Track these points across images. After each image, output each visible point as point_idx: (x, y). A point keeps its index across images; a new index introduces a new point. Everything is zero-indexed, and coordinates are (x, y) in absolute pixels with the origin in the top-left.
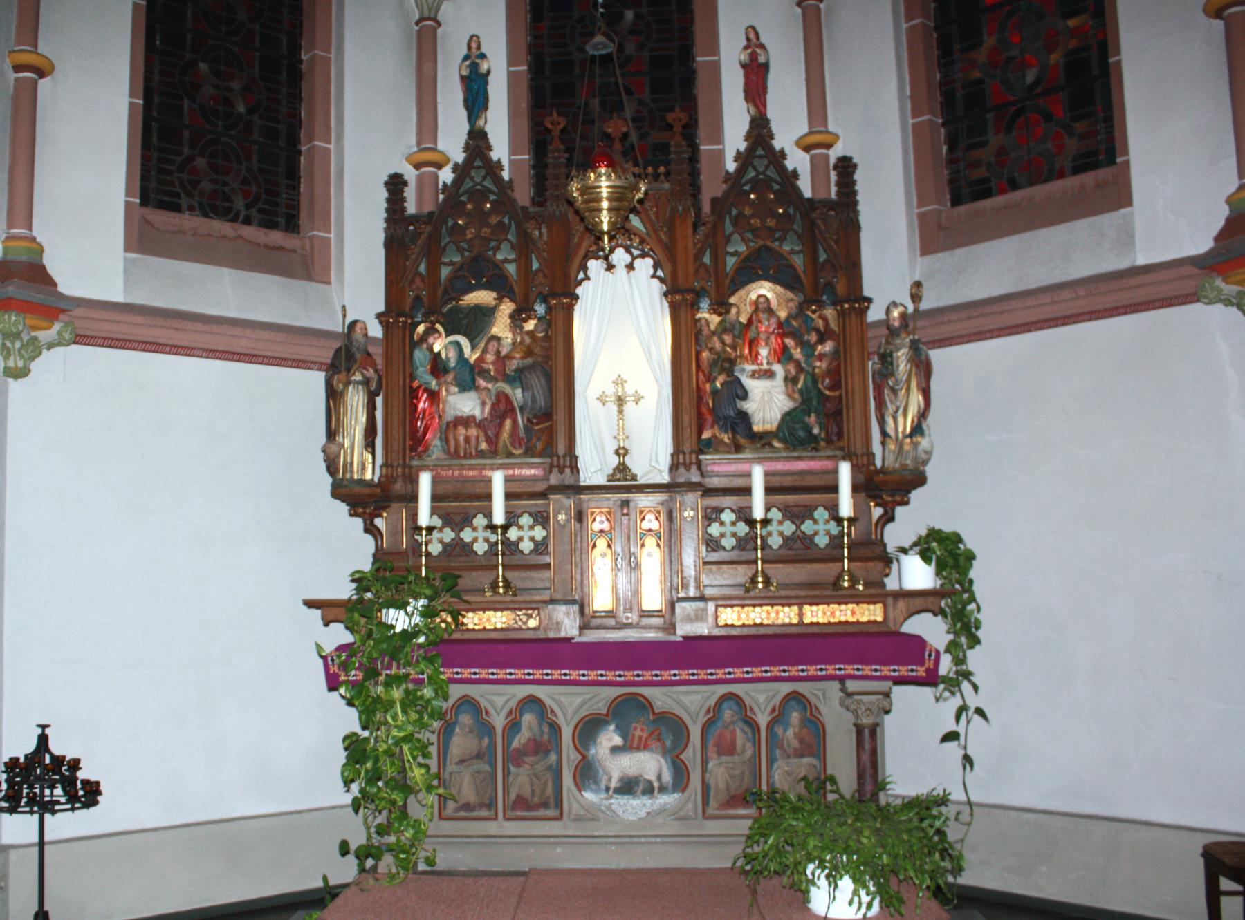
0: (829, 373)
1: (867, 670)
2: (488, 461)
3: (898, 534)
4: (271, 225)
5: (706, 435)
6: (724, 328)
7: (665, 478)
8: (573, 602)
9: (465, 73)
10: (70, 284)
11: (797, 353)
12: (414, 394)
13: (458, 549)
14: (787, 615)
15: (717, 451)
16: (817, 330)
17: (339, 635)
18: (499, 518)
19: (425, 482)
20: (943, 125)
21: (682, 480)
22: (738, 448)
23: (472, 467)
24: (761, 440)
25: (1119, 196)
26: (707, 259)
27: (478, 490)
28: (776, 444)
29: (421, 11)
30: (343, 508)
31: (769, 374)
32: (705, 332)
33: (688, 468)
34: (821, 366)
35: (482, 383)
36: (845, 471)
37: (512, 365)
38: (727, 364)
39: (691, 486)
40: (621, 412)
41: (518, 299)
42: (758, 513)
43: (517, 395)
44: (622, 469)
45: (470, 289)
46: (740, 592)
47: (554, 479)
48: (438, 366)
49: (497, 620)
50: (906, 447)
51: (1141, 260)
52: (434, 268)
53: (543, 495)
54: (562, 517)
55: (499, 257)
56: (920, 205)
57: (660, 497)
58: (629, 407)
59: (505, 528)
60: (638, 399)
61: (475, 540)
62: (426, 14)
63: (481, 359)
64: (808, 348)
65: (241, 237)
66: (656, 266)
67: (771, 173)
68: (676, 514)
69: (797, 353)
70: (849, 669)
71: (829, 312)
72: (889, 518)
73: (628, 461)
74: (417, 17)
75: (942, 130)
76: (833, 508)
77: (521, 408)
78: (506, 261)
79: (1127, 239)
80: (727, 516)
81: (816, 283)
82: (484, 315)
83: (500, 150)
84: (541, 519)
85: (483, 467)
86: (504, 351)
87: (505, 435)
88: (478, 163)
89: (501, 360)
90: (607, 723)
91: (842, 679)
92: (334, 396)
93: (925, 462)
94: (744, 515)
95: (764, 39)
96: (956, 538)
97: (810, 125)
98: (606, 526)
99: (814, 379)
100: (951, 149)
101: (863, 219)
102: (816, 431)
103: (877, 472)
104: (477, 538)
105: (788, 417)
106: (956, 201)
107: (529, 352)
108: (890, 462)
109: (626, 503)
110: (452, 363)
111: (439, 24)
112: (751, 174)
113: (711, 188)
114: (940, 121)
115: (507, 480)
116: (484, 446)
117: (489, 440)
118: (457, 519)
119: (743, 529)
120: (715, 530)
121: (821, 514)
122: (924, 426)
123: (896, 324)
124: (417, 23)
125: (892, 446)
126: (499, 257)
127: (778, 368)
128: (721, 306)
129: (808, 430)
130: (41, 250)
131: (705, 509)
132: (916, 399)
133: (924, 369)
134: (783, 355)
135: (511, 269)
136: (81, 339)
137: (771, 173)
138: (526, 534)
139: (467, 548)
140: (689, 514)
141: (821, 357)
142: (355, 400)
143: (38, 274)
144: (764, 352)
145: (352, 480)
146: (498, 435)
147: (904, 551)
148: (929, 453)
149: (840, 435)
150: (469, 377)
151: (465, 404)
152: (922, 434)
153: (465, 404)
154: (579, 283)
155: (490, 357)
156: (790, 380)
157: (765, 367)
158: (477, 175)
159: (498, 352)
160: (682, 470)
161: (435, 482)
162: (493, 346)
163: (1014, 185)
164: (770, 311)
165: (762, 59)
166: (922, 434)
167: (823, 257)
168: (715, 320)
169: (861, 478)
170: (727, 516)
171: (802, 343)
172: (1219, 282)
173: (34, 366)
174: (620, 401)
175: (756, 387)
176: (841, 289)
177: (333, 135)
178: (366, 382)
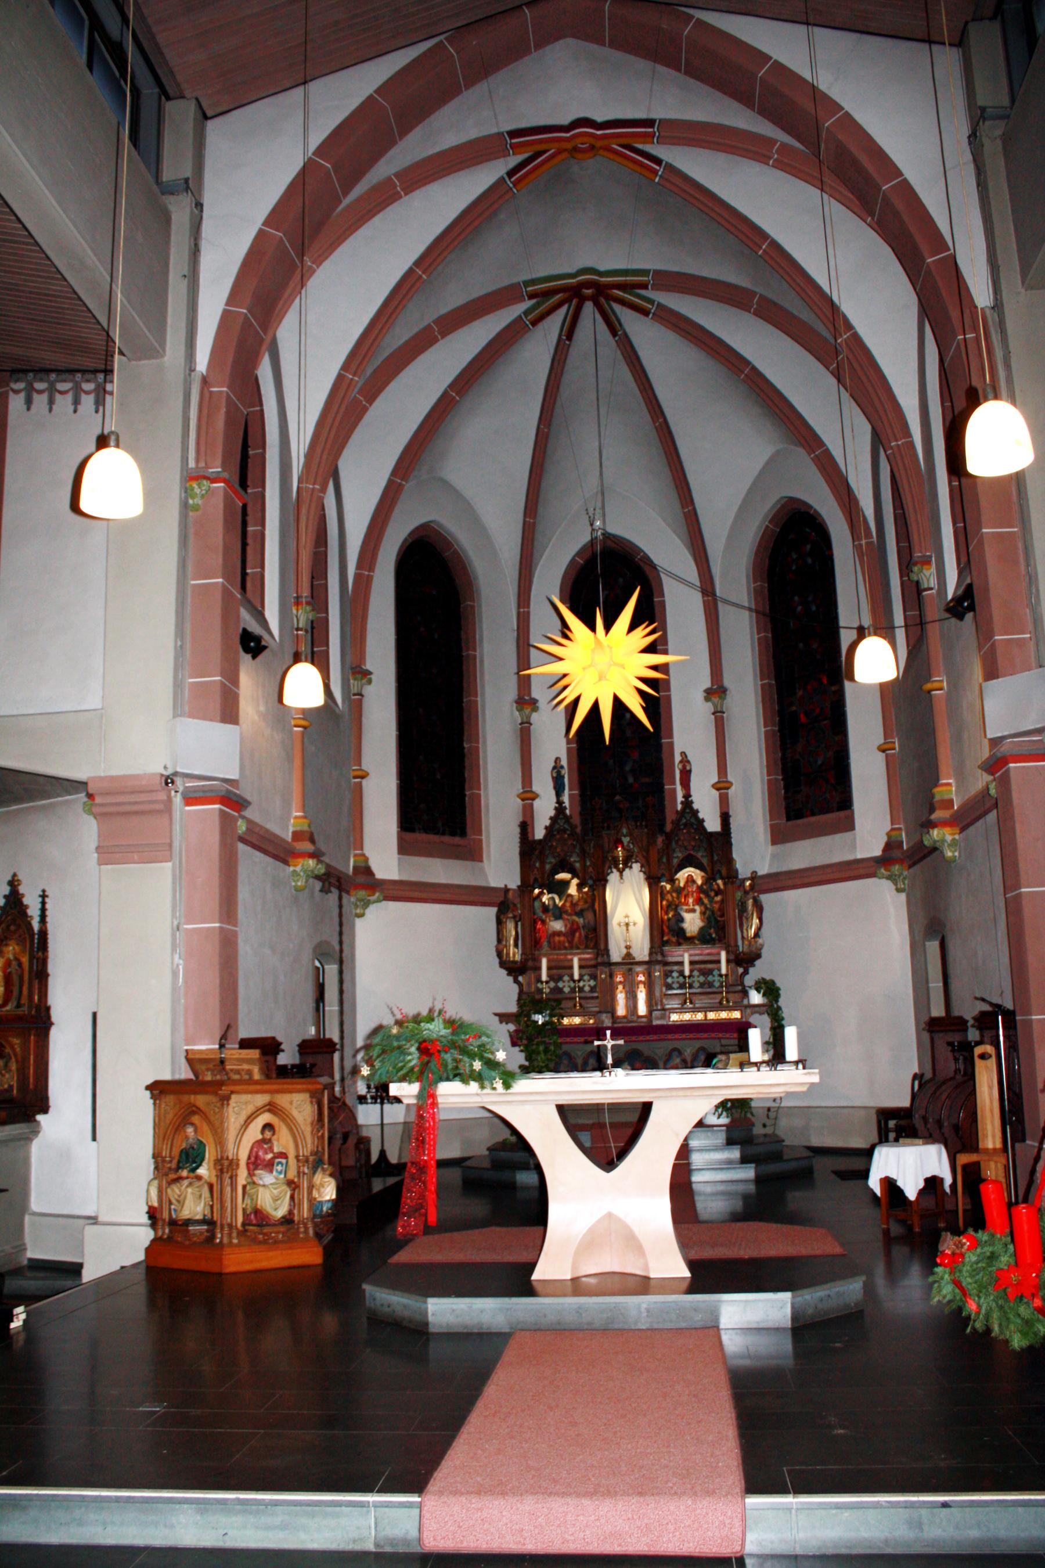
0: (720, 910)
1: (728, 1035)
2: (568, 952)
3: (749, 980)
4: (453, 834)
5: (665, 938)
6: (673, 889)
7: (647, 959)
8: (608, 1012)
9: (555, 775)
10: (380, 873)
11: (706, 901)
12: (535, 922)
13: (558, 990)
14: (700, 1016)
15: (671, 945)
16: (714, 890)
17: (512, 1027)
18: (576, 977)
19: (544, 962)
20: (782, 780)
21: (654, 959)
22: (679, 944)
23: (562, 954)
24: (690, 940)
25: (849, 825)
26: (664, 860)
27: (566, 964)
28: (697, 942)
29: (522, 719)
30: (504, 972)
31: (693, 911)
32: (665, 892)
33: (657, 954)
34: (716, 906)
35: (565, 916)
36: (723, 955)
37: (579, 908)
38: (674, 906)
39: (658, 962)
40: (627, 930)
41: (580, 875)
42: (687, 973)
43: (581, 921)
44: (628, 955)
45: (558, 873)
46: (680, 1006)
47: (600, 960)
48: (545, 909)
49: (577, 1020)
50: (753, 943)
51: (859, 856)
52: (543, 864)
53: (595, 966)
54: (603, 976)
55: (572, 860)
56: (771, 820)
57: (645, 967)
58: (631, 928)
59: (579, 981)
60: (635, 924)
61: (564, 986)
62: (525, 720)
63: (564, 905)
64: (711, 901)
65: (442, 842)
66: (642, 866)
67: (693, 820)
68: (652, 974)
69: (706, 901)
70: (720, 1035)
71: (720, 882)
72: (746, 972)
73: (631, 951)
74: (520, 721)
75: (782, 782)
76: (571, 976)
77: (583, 927)
78: (575, 861)
79: (853, 847)
80: (675, 974)
81: (712, 870)
82: (566, 884)
83: (567, 804)
84: (594, 977)
85: (566, 954)
86: (574, 901)
87: (576, 939)
88: (561, 816)
89: (574, 905)
90: (624, 1061)
91: (719, 1038)
92: (500, 922)
93: (760, 949)
94: (681, 973)
95: (689, 758)
96: (773, 982)
97: (719, 778)
98: (622, 979)
99: (713, 912)
100: (786, 792)
101: (733, 840)
102: (714, 936)
103: (740, 953)
104: (566, 986)
105: (701, 929)
106: (788, 819)
107: (586, 902)
108: (746, 949)
109: (630, 970)
110: (551, 907)
111: (531, 724)
112: (684, 821)
113: (670, 817)
114: (781, 777)
115: (580, 960)
116: (567, 945)
117: (569, 942)
118: (556, 977)
119: (681, 979)
120: (669, 980)
121: (566, 978)
122: (760, 933)
123: (748, 889)
124: (521, 724)
125: (746, 942)
126: (572, 860)
127: (697, 908)
128: (672, 881)
129: (710, 935)
130: (367, 859)
131: (665, 971)
132: (756, 921)
133: (759, 908)
134: (699, 901)
135: (577, 865)
136: (387, 898)
137: (693, 820)
138: (587, 983)
139: (560, 990)
140: (657, 974)
141: (716, 902)
142: (510, 926)
143: (368, 871)
144: (691, 900)
145: (509, 961)
146: (573, 940)
147: (750, 987)
148: (762, 946)
149: (725, 937)
150: (559, 913)
151: (558, 926)
152: (759, 937)
153: (558, 926)
154: (608, 874)
155: (568, 904)
156: (703, 913)
157: (691, 907)
158: (561, 822)
159: (572, 902)
160: (654, 955)
161: (549, 961)
162: (569, 899)
163: (813, 814)
164: (694, 882)
165: (688, 768)
166: (759, 937)
167: (716, 858)
168: (668, 887)
169: (732, 957)
170: (675, 974)
171: (707, 896)
172: (882, 870)
173: (367, 911)
174: (627, 925)
175: (687, 917)
176: (724, 872)
177: (482, 786)
178: (514, 917)
